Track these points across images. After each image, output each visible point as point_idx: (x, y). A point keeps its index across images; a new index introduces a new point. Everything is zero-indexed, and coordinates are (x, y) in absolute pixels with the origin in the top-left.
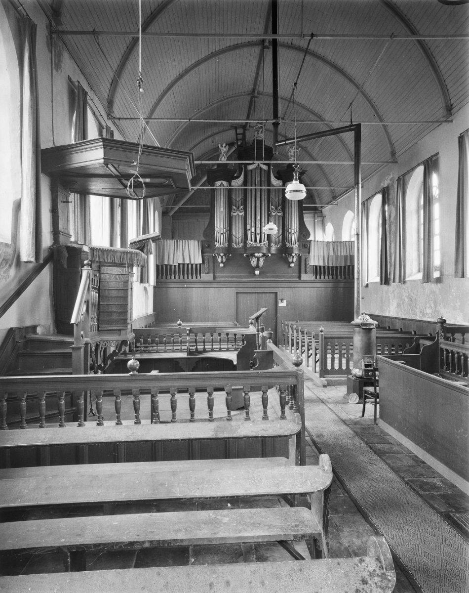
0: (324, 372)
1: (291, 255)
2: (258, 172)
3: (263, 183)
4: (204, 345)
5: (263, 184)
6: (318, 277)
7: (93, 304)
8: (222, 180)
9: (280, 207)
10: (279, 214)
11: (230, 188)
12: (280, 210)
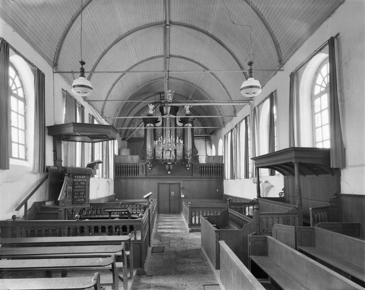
0: (191, 225)
1: (187, 163)
4: (136, 210)
5: (172, 126)
6: (203, 175)
7: (69, 192)
8: (151, 123)
9: (181, 138)
11: (155, 128)
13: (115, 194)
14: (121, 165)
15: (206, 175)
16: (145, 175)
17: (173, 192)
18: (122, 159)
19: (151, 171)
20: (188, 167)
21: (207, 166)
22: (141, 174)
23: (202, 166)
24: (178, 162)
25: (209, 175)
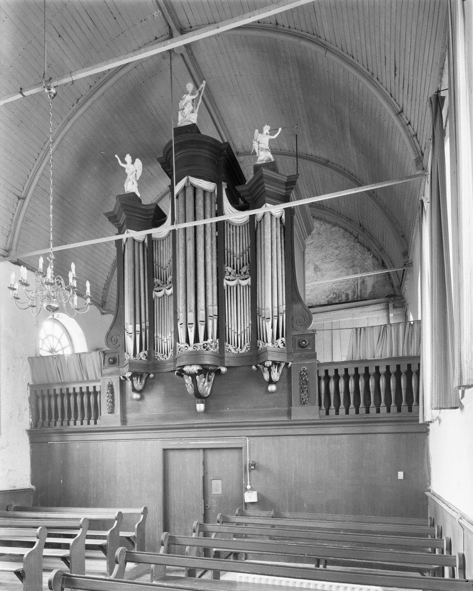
1: (263, 364)
2: (268, 218)
3: (202, 229)
6: (332, 411)
9: (244, 269)
10: (244, 283)
12: (245, 273)
13: (33, 487)
14: (68, 386)
15: (347, 413)
16: (119, 418)
17: (219, 482)
18: (54, 372)
19: (140, 403)
20: (271, 382)
21: (351, 372)
22: (108, 418)
23: (331, 373)
24: (232, 364)
25: (362, 410)
